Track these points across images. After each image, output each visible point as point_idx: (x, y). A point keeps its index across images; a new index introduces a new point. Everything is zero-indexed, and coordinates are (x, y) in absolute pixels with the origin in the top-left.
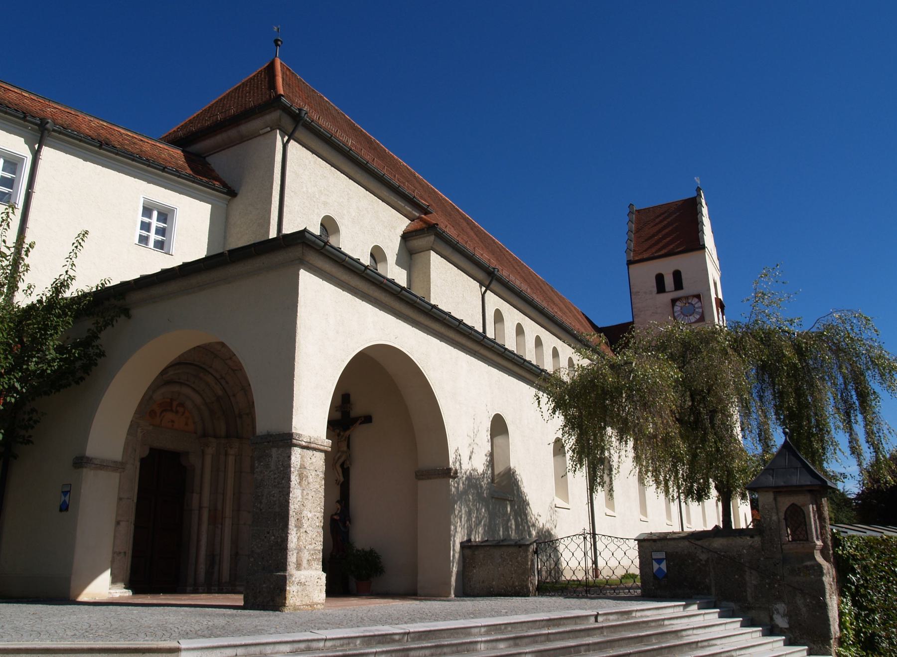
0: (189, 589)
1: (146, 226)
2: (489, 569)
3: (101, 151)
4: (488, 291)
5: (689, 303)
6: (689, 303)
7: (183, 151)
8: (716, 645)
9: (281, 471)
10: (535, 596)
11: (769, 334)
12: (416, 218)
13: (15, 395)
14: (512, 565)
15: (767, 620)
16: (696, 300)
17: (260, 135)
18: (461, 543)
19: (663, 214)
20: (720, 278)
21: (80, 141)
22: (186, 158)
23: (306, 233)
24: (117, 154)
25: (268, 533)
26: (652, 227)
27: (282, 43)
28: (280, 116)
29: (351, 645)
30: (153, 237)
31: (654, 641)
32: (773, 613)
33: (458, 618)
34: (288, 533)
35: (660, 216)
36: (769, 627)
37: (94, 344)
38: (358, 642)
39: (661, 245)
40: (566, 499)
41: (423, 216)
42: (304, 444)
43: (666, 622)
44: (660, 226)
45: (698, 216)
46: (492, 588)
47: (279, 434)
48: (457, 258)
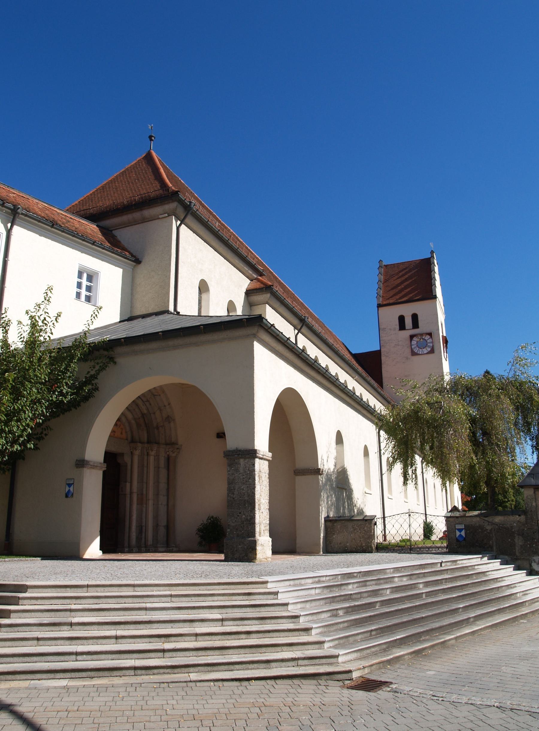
0: (126, 549)
1: (79, 285)
3: (53, 229)
4: (300, 333)
5: (423, 339)
6: (423, 339)
7: (97, 226)
8: (505, 580)
10: (375, 552)
11: (521, 384)
13: (42, 417)
14: (360, 532)
15: (528, 566)
16: (428, 337)
17: (159, 218)
18: (325, 518)
19: (405, 269)
20: (445, 320)
21: (39, 221)
22: (101, 232)
23: (264, 319)
24: (63, 232)
25: (240, 513)
26: (396, 279)
27: (155, 138)
28: (176, 207)
29: (337, 579)
30: (84, 292)
31: (474, 578)
32: (532, 562)
33: (371, 564)
34: (255, 513)
35: (403, 270)
36: (530, 570)
37: (93, 382)
38: (339, 577)
39: (403, 293)
40: (369, 488)
41: (259, 277)
42: (261, 456)
43: (476, 567)
44: (403, 279)
45: (432, 273)
47: (246, 450)
48: (282, 309)
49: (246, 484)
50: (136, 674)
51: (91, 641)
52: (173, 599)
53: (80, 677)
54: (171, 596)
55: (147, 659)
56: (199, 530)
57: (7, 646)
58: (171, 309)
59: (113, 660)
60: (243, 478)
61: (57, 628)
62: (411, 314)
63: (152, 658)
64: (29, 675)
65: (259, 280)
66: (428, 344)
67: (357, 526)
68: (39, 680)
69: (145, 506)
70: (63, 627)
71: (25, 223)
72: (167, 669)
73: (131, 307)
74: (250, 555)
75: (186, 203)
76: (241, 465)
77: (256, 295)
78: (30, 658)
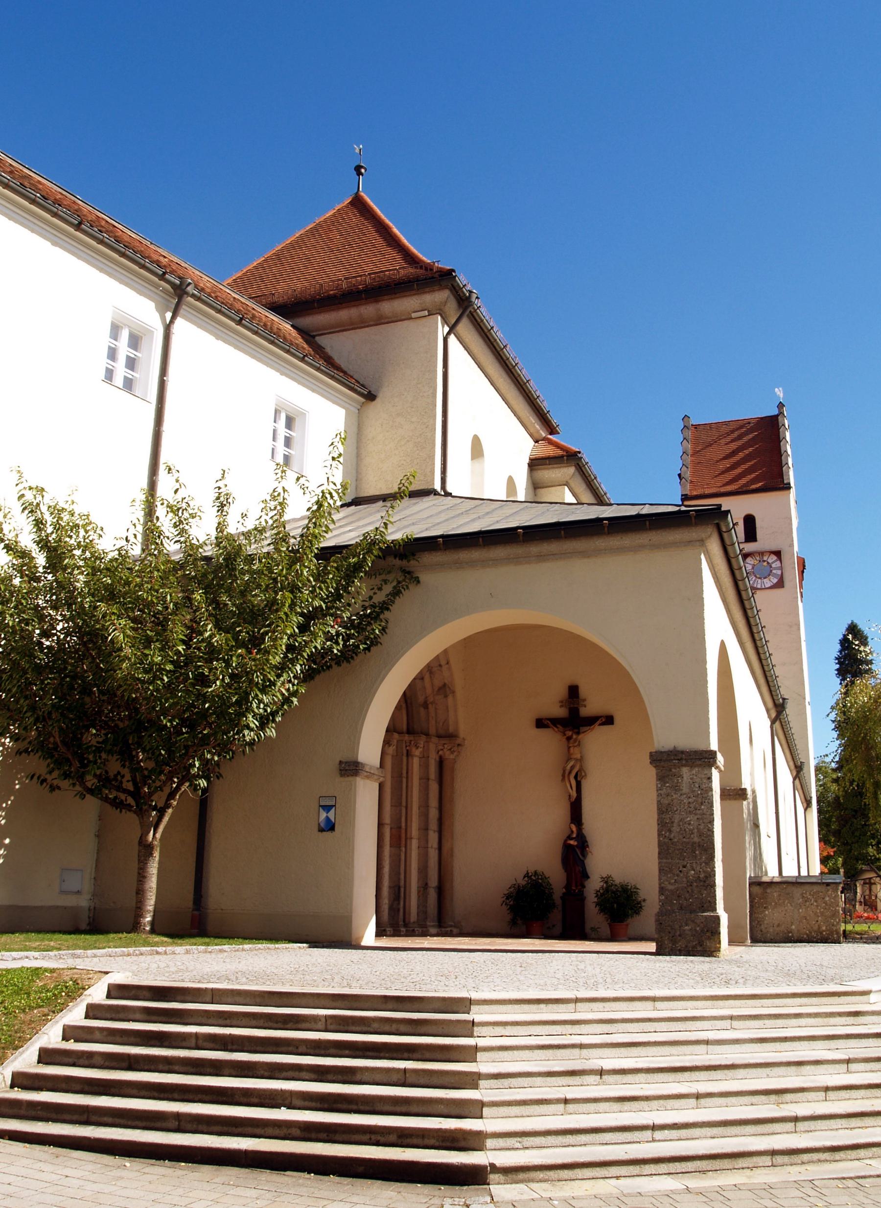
2: (786, 910)
9: (698, 794)
12: (541, 439)
16: (773, 558)
17: (411, 318)
25: (684, 867)
41: (550, 437)
46: (791, 932)
49: (696, 814)
50: (774, 1164)
51: (655, 1104)
52: (736, 1024)
53: (684, 1171)
54: (731, 1018)
55: (768, 1134)
56: (508, 896)
57: (513, 1115)
58: (437, 486)
59: (714, 1138)
60: (689, 803)
61: (576, 1080)
62: (743, 516)
63: (778, 1133)
64: (598, 1169)
65: (550, 442)
66: (774, 571)
67: (810, 894)
68: (617, 1178)
69: (403, 849)
70: (587, 1077)
71: (192, 311)
72: (824, 1152)
73: (356, 480)
74: (708, 944)
75: (463, 292)
76: (685, 778)
77: (548, 469)
78: (574, 1136)
